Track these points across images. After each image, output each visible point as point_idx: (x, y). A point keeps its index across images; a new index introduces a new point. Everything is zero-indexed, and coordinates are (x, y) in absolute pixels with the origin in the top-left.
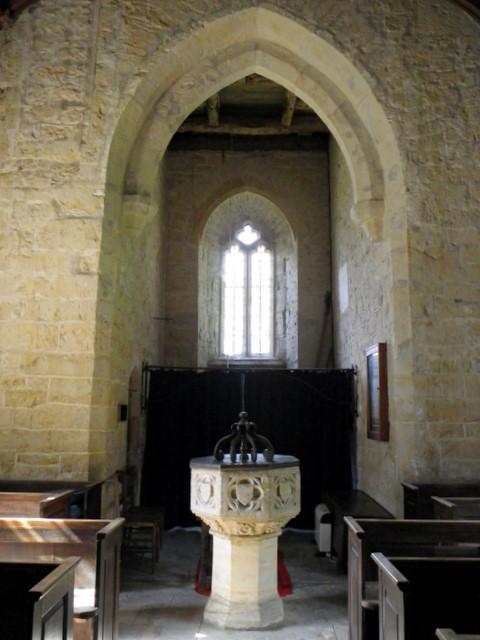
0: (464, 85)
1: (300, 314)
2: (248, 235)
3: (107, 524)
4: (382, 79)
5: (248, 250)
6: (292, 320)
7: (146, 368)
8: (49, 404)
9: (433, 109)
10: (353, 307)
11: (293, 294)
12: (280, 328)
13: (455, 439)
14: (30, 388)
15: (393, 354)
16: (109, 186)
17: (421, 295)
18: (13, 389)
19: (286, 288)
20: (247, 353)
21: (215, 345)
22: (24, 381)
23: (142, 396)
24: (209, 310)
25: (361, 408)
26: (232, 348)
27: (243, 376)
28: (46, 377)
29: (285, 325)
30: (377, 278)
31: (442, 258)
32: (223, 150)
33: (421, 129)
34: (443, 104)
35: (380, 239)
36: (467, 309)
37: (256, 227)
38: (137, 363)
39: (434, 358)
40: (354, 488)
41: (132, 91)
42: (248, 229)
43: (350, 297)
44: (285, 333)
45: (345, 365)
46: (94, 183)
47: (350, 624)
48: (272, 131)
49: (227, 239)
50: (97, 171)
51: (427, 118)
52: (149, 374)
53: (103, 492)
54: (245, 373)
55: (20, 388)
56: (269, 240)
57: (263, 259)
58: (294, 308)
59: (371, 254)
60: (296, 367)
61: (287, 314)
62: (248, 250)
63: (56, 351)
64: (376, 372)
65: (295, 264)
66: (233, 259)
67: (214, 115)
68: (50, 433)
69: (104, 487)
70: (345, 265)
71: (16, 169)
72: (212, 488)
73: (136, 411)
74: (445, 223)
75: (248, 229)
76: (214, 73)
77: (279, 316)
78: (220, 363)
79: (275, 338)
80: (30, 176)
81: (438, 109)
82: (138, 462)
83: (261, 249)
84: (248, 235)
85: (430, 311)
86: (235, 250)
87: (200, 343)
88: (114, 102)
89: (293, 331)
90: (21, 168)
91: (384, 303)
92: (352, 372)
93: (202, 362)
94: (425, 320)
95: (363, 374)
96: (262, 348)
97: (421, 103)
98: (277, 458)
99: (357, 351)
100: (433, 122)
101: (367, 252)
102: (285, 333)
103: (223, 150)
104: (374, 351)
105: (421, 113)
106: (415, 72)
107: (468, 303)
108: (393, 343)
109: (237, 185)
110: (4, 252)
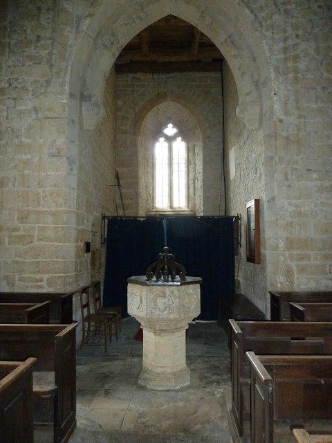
0: (317, 18)
1: (204, 180)
2: (170, 130)
3: (65, 327)
4: (257, 14)
5: (170, 139)
6: (199, 184)
7: (104, 217)
8: (36, 243)
9: (294, 35)
10: (238, 176)
11: (200, 168)
12: (191, 190)
13: (305, 262)
14: (24, 233)
15: (265, 206)
16: (72, 96)
17: (283, 166)
18: (13, 234)
19: (195, 164)
20: (171, 207)
21: (150, 202)
22: (20, 229)
23: (102, 236)
24: (146, 179)
25: (243, 241)
26: (161, 203)
27: (165, 222)
28: (33, 225)
29: (195, 188)
30: (254, 155)
31: (298, 141)
32: (153, 73)
33: (285, 50)
34: (300, 32)
35: (260, 126)
36: (315, 176)
37: (175, 125)
38: (98, 214)
39: (292, 209)
40: (237, 293)
41: (85, 28)
42: (170, 126)
43: (236, 169)
44: (194, 193)
45: (233, 213)
46: (62, 93)
47: (233, 385)
48: (185, 59)
49: (158, 133)
50: (62, 85)
51: (290, 42)
52: (107, 221)
53: (74, 300)
54: (167, 219)
55: (17, 233)
56: (184, 133)
57: (180, 146)
58: (200, 177)
59: (250, 140)
60: (202, 214)
61: (196, 181)
62: (170, 139)
63: (40, 208)
64: (253, 218)
65: (201, 148)
66: (160, 148)
67: (145, 48)
68: (38, 262)
69: (74, 296)
70: (233, 148)
71: (8, 85)
72: (141, 299)
73: (97, 244)
74: (300, 117)
75: (170, 126)
76: (142, 15)
77: (191, 182)
78: (154, 213)
79: (188, 197)
80: (17, 90)
81: (297, 36)
82: (101, 277)
83: (179, 139)
84: (170, 130)
85: (289, 176)
86: (162, 139)
87: (140, 201)
88: (72, 36)
89: (200, 192)
90: (10, 85)
91: (258, 173)
92: (238, 218)
93: (142, 213)
94: (286, 183)
95: (245, 218)
96: (181, 203)
97: (285, 31)
98: (189, 279)
99: (242, 205)
100: (294, 45)
101: (247, 139)
102: (194, 193)
103: (153, 73)
104: (251, 204)
105: (286, 39)
106: (282, 10)
107: (315, 171)
108: (264, 199)
109: (161, 97)
110: (3, 142)
